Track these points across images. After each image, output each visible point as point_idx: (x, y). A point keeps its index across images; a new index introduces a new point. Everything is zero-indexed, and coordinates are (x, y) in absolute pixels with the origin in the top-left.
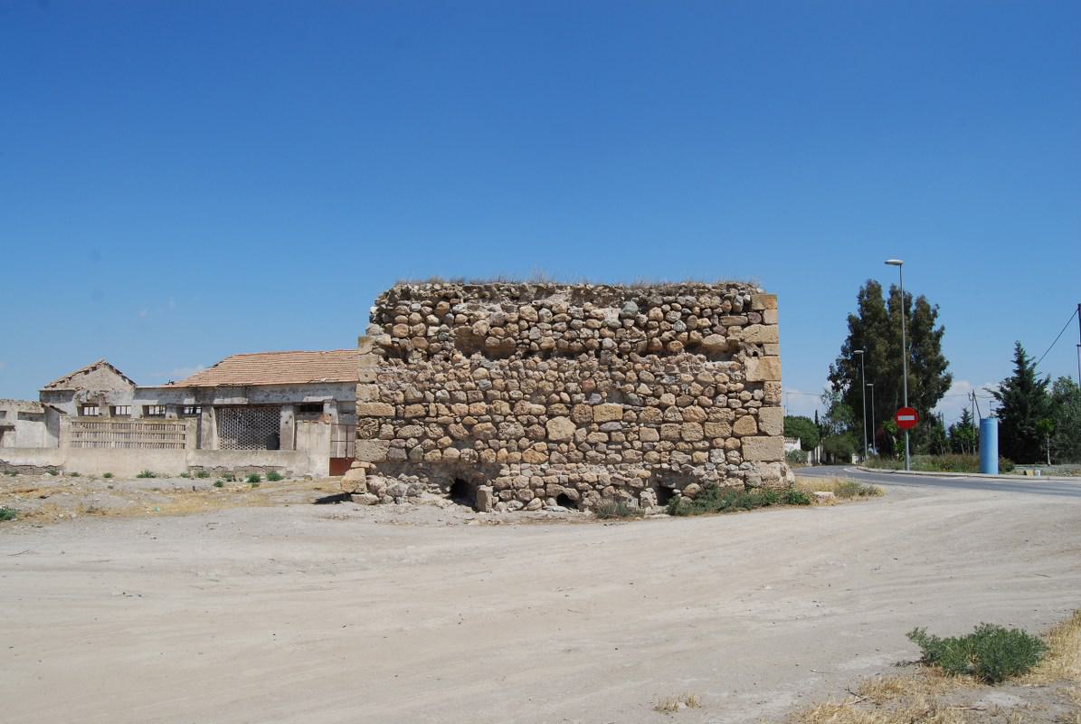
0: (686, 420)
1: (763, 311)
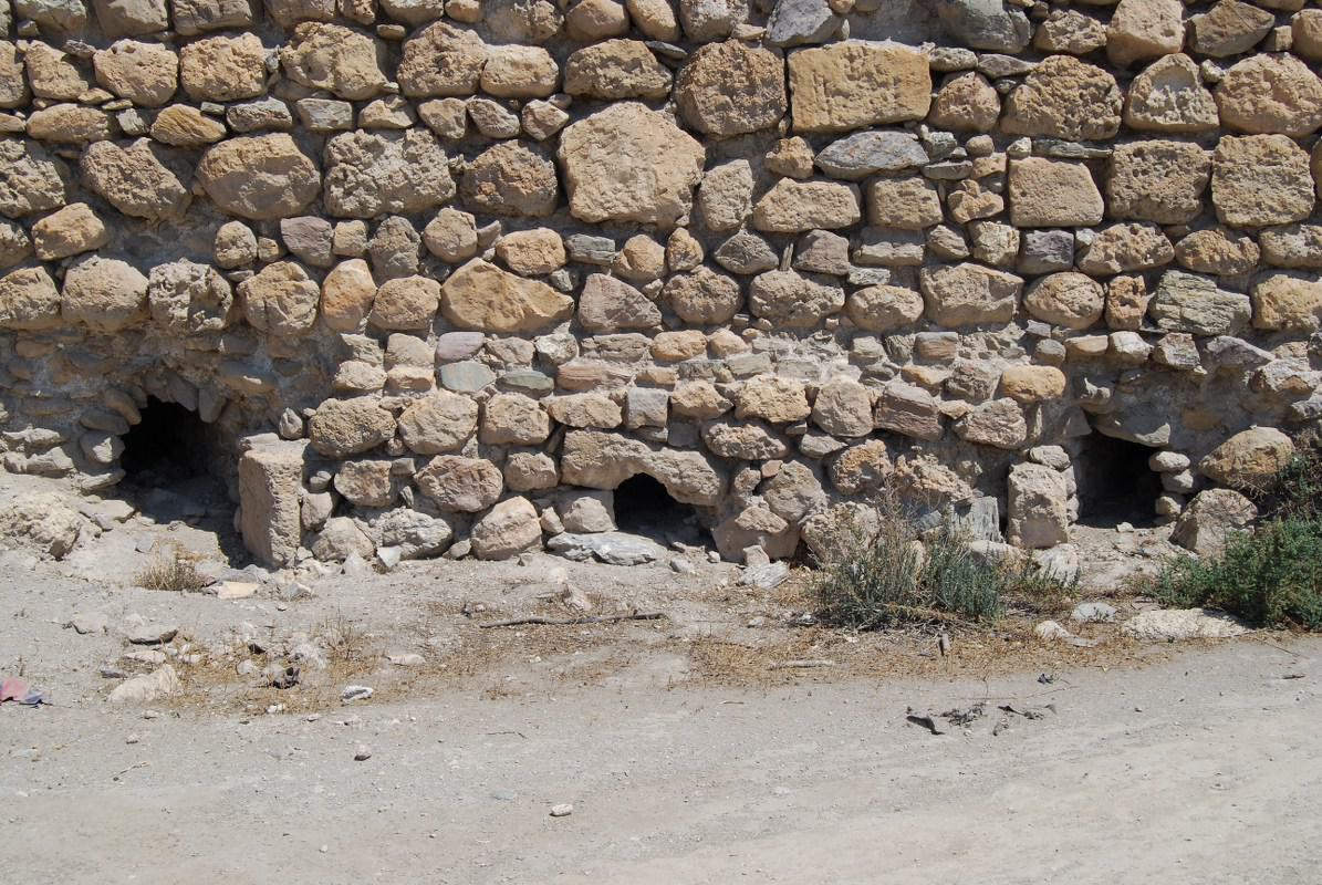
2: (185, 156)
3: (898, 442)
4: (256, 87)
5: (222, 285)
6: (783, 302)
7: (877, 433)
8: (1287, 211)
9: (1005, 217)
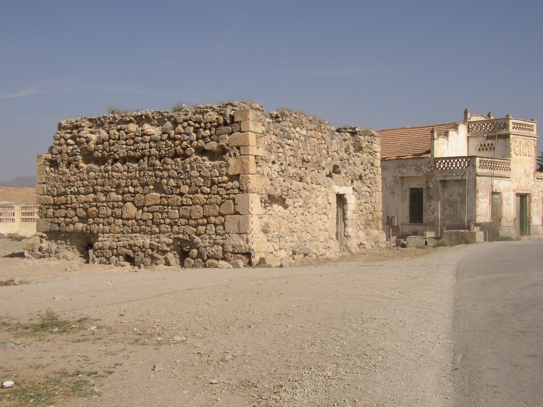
0: (193, 204)
1: (241, 122)
2: (86, 209)
3: (153, 250)
4: (92, 201)
5: (88, 227)
6: (143, 230)
7: (150, 248)
8: (199, 216)
9: (168, 218)
